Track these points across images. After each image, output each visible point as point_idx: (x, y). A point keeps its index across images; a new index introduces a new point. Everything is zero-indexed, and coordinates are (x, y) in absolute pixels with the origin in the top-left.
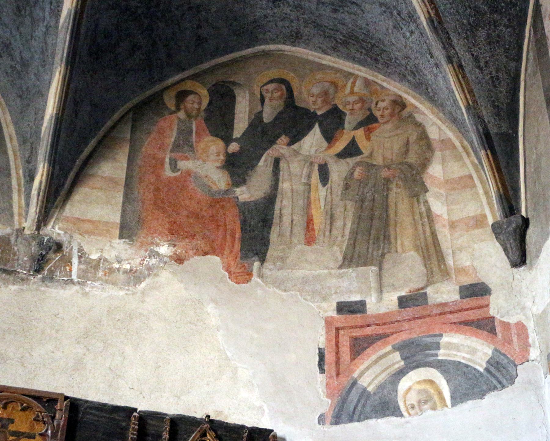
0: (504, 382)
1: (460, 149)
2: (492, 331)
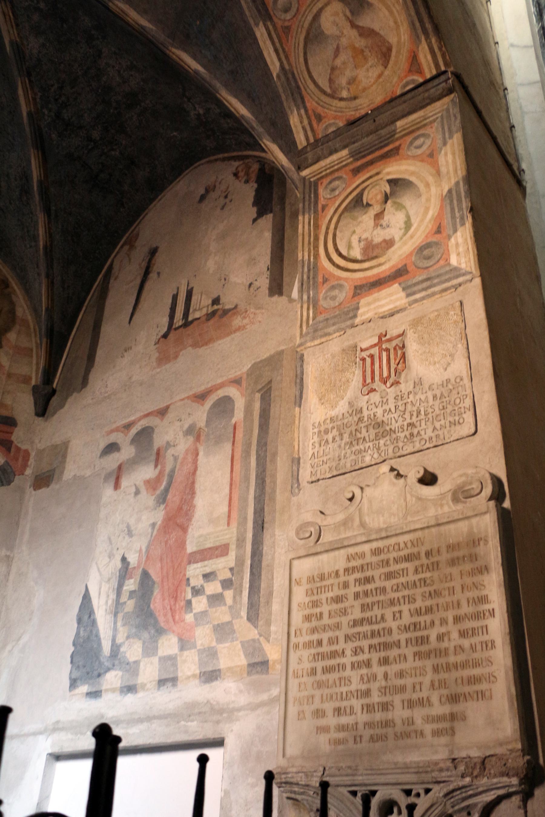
0: (5, 482)
1: (32, 330)
2: (9, 450)
